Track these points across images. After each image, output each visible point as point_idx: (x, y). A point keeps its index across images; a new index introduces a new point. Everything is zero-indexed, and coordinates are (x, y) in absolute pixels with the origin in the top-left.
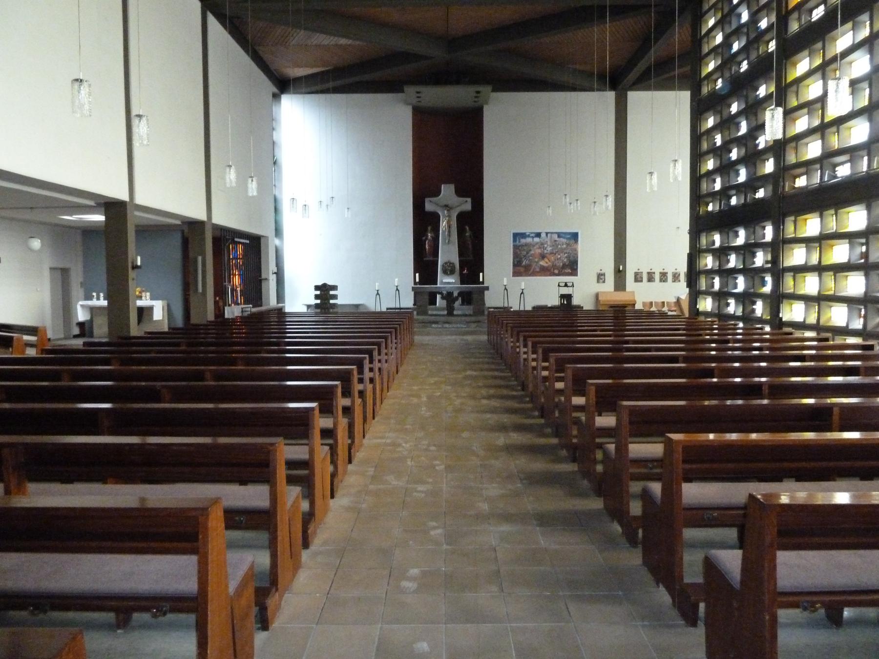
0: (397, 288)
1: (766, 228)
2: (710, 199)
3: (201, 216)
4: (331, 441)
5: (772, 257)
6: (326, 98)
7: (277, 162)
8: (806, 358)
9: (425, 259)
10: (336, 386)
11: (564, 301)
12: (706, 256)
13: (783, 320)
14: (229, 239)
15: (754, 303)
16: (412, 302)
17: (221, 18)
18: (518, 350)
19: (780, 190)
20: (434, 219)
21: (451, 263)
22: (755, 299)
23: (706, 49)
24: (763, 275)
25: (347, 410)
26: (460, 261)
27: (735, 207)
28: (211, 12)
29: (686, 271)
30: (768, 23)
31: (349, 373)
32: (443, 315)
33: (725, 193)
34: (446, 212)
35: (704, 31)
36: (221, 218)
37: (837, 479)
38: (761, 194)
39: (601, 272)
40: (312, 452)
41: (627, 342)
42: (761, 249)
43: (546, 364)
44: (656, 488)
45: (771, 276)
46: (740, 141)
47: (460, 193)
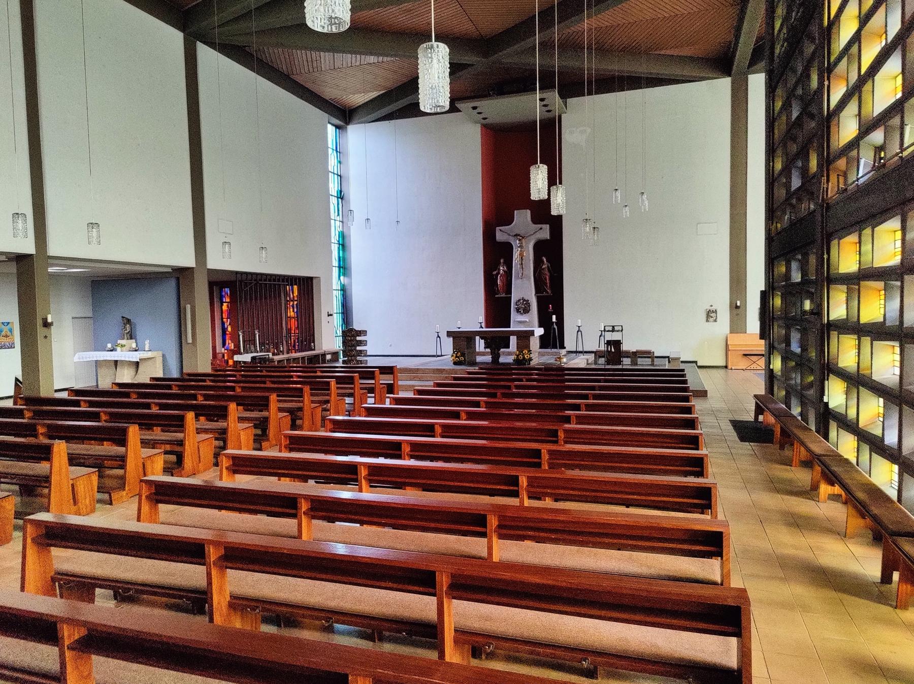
0: (438, 335)
3: (187, 260)
6: (906, 125)
11: (611, 349)
21: (525, 300)
34: (518, 242)
39: (711, 308)
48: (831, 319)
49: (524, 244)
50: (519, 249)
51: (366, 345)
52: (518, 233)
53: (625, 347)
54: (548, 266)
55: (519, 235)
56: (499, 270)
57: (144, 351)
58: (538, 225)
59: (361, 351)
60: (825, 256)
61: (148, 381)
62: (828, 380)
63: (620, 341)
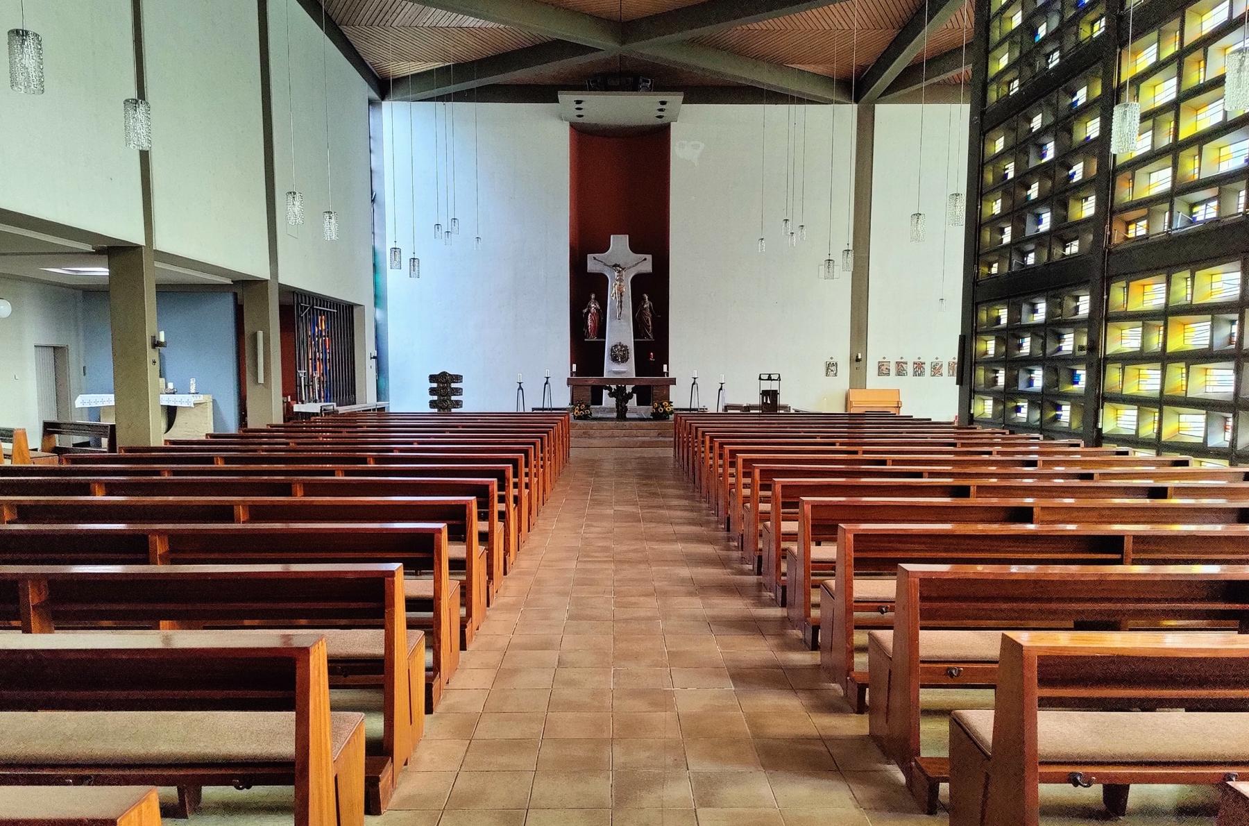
0: (520, 386)
1: (1081, 298)
3: (262, 272)
5: (1090, 340)
7: (377, 198)
8: (1169, 491)
9: (586, 340)
10: (439, 530)
11: (767, 400)
12: (986, 339)
14: (306, 308)
15: (1058, 407)
16: (568, 400)
18: (703, 455)
20: (599, 283)
21: (622, 346)
22: (1060, 402)
23: (996, 35)
24: (1074, 367)
25: (458, 565)
27: (1033, 268)
32: (612, 419)
34: (616, 274)
36: (296, 274)
38: (1074, 248)
40: (389, 643)
44: (886, 636)
45: (1087, 369)
46: (1045, 171)
47: (635, 247)
48: (1107, 353)
50: (618, 283)
51: (462, 395)
52: (618, 264)
53: (782, 401)
54: (650, 305)
55: (619, 266)
56: (590, 307)
57: (189, 393)
59: (456, 401)
60: (1105, 297)
61: (204, 438)
62: (1102, 408)
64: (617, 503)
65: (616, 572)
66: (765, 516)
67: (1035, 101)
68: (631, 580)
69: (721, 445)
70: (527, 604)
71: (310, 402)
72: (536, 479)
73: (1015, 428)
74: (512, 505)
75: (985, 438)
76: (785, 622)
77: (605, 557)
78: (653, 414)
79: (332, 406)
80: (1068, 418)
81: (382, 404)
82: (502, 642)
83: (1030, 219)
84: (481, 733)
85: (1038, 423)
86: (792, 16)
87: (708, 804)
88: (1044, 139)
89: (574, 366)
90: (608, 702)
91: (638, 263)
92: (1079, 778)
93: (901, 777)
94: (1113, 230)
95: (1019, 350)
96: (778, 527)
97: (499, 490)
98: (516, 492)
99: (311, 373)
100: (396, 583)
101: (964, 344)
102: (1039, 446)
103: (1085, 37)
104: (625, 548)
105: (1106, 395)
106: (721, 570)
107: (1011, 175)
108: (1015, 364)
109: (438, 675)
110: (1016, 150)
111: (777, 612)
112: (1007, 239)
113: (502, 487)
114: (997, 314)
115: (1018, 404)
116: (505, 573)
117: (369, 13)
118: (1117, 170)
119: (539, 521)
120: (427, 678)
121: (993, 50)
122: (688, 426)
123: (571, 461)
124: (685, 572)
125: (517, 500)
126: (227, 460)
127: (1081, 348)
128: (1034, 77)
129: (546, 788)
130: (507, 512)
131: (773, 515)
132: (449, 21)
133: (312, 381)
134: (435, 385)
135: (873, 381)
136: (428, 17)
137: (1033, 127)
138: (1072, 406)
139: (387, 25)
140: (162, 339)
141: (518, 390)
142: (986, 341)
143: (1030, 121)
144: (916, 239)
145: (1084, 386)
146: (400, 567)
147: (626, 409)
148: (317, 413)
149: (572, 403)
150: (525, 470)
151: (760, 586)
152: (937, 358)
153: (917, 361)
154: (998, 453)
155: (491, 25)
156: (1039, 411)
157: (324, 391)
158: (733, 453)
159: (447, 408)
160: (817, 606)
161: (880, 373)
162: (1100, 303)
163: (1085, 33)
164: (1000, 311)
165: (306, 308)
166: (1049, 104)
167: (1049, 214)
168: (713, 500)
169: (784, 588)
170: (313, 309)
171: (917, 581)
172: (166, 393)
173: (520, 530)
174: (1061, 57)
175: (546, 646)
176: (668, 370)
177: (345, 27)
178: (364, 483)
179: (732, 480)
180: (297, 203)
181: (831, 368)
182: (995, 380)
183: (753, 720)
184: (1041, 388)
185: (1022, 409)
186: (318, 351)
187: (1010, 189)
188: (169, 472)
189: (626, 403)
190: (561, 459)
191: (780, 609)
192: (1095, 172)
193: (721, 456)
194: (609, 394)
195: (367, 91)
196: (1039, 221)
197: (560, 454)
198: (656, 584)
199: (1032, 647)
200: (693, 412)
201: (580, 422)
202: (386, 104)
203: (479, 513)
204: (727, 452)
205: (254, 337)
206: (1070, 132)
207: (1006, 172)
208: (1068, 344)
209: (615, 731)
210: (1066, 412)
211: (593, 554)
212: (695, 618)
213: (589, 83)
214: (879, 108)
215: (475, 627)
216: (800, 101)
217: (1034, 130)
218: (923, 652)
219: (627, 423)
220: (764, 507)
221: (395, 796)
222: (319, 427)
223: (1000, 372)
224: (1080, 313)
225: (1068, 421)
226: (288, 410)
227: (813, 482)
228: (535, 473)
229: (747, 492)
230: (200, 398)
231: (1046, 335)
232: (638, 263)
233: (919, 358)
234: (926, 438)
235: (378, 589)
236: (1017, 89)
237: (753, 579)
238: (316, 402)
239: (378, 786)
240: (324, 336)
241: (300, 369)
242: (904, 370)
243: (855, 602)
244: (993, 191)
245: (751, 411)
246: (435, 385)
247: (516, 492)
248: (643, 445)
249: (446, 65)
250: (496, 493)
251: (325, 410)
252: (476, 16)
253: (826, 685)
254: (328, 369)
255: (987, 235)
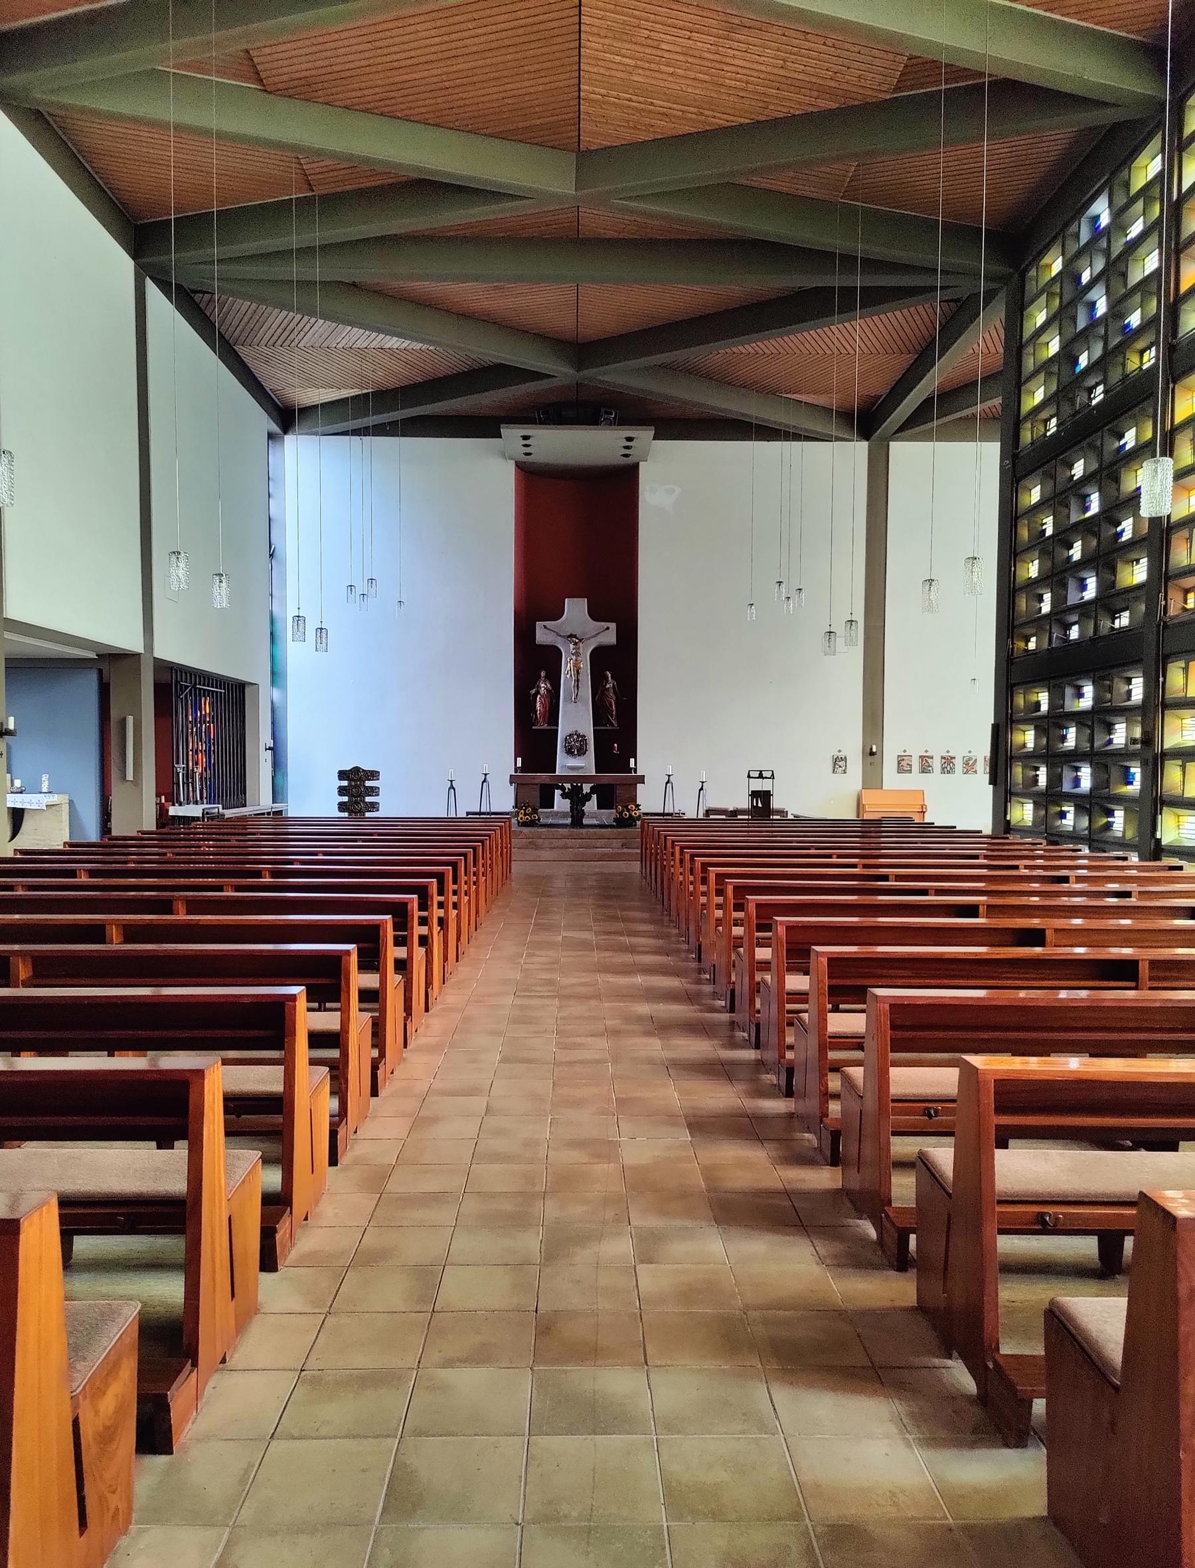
0: (452, 784)
1: (1134, 681)
2: (1033, 631)
3: (132, 641)
4: (335, 1053)
5: (1144, 732)
9: (533, 727)
10: (348, 953)
11: (757, 803)
12: (1024, 729)
13: (1164, 843)
14: (187, 687)
15: (1110, 813)
16: (513, 804)
17: (165, 286)
19: (1160, 613)
21: (579, 736)
23: (1029, 364)
25: (368, 996)
26: (596, 733)
27: (1077, 643)
28: (153, 279)
29: (988, 754)
30: (1142, 319)
31: (376, 928)
33: (1060, 616)
34: (572, 646)
35: (1027, 333)
37: (1148, 1055)
38: (1124, 620)
41: (885, 878)
42: (1123, 719)
43: (741, 915)
44: (943, 1154)
46: (1088, 528)
47: (596, 614)
48: (1166, 747)
49: (581, 651)
50: (574, 657)
51: (378, 795)
53: (776, 803)
55: (575, 636)
56: (539, 687)
57: (41, 793)
58: (603, 623)
61: (61, 847)
62: (1161, 814)
63: (770, 791)
64: (568, 927)
65: (560, 1008)
66: (737, 942)
67: (1075, 444)
68: (576, 1018)
69: (693, 856)
70: (451, 1046)
71: (188, 804)
72: (467, 898)
73: (1055, 838)
74: (436, 928)
75: (1025, 850)
76: (760, 1065)
77: (549, 991)
78: (616, 820)
79: (218, 808)
80: (1122, 825)
81: (278, 806)
82: (422, 1087)
83: (1072, 585)
84: (394, 1186)
85: (1087, 832)
86: (786, 338)
87: (650, 1261)
88: (1088, 490)
89: (519, 760)
90: (542, 1153)
91: (599, 633)
92: (1048, 1218)
93: (873, 1233)
94: (1169, 600)
95: (1063, 743)
96: (752, 954)
97: (420, 910)
98: (441, 913)
99: (191, 768)
100: (297, 1008)
101: (997, 738)
102: (1088, 859)
103: (1133, 369)
104: (574, 981)
105: (1164, 798)
106: (686, 1007)
107: (1049, 532)
108: (1058, 760)
109: (344, 1121)
110: (1054, 501)
111: (750, 1055)
112: (1046, 608)
113: (423, 906)
114: (1035, 699)
115: (1063, 809)
116: (427, 1010)
117: (271, 331)
118: (1172, 528)
119: (471, 950)
120: (331, 1124)
121: (1025, 383)
122: (656, 833)
123: (513, 877)
124: (644, 1009)
125: (442, 922)
126: (92, 873)
127: (1134, 741)
128: (1074, 415)
129: (464, 1244)
130: (430, 937)
131: (746, 939)
132: (368, 341)
133: (192, 778)
134: (345, 783)
135: (891, 778)
136: (342, 336)
137: (1074, 475)
138: (1126, 810)
139: (292, 345)
140: (11, 726)
141: (449, 789)
142: (1024, 731)
143: (1071, 467)
144: (929, 608)
145: (1139, 787)
146: (303, 990)
147: (583, 813)
148: (198, 818)
149: (516, 806)
150: (452, 887)
151: (733, 1025)
152: (970, 752)
153: (945, 754)
154: (1026, 867)
155: (418, 346)
156: (1087, 818)
157: (206, 790)
158: (705, 866)
159: (360, 811)
160: (791, 1047)
161: (900, 770)
162: (1155, 685)
163: (1133, 363)
164: (1040, 694)
165: (187, 687)
166: (1092, 446)
167: (1094, 579)
168: (683, 926)
169: (758, 1026)
170: (196, 689)
171: (887, 1007)
172: (12, 793)
173: (445, 959)
174: (1105, 392)
175: (472, 1092)
176: (636, 765)
177: (241, 347)
178: (255, 900)
179: (703, 900)
180: (182, 565)
181: (838, 763)
182: (1035, 780)
183: (709, 1172)
184: (1089, 789)
185: (1068, 814)
186: (201, 741)
187: (1049, 547)
188: (23, 886)
189: (584, 805)
190: (500, 876)
191: (753, 1051)
192: (1147, 531)
193: (692, 871)
194: (562, 795)
195: (265, 423)
196: (1083, 587)
197: (498, 870)
198: (609, 1023)
199: (987, 1070)
200: (668, 817)
201: (526, 830)
202: (289, 439)
203: (396, 938)
204: (698, 866)
205: (123, 723)
206: (1117, 480)
207: (1044, 527)
208: (1120, 736)
209: (548, 1184)
210: (1119, 819)
211: (533, 988)
212: (651, 1061)
213: (539, 415)
214: (895, 447)
215: (389, 1071)
216: (797, 437)
217: (1075, 478)
218: (895, 1090)
219: (584, 831)
220: (738, 931)
221: (293, 1252)
222: (200, 834)
223: (1041, 769)
224: (1133, 698)
225: (1122, 829)
226: (162, 812)
227: (793, 900)
228: (466, 891)
229: (719, 913)
230: (54, 799)
231: (1093, 723)
232: (599, 633)
233: (948, 752)
234: (944, 849)
235: (279, 1012)
236: (1055, 429)
237: (725, 1017)
238: (197, 804)
239: (275, 1238)
240: (209, 722)
241: (178, 763)
242: (929, 766)
243: (830, 1037)
244: (1029, 549)
245: (739, 817)
246: (345, 783)
247: (441, 913)
248: (603, 858)
249: (364, 392)
250: (417, 914)
251: (207, 813)
252: (399, 335)
253: (798, 1135)
254: (212, 762)
255: (1022, 603)
